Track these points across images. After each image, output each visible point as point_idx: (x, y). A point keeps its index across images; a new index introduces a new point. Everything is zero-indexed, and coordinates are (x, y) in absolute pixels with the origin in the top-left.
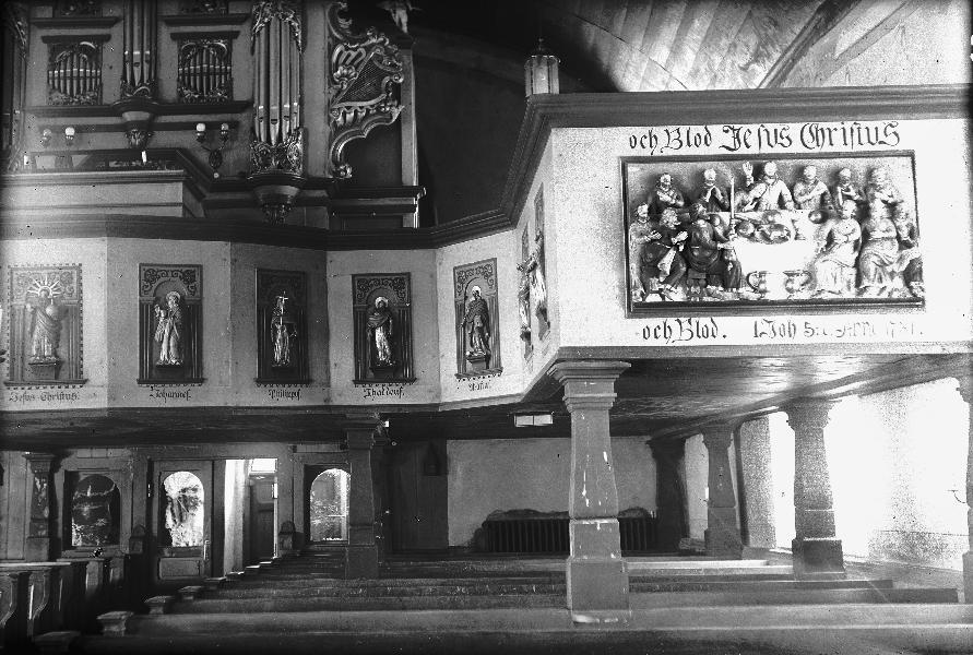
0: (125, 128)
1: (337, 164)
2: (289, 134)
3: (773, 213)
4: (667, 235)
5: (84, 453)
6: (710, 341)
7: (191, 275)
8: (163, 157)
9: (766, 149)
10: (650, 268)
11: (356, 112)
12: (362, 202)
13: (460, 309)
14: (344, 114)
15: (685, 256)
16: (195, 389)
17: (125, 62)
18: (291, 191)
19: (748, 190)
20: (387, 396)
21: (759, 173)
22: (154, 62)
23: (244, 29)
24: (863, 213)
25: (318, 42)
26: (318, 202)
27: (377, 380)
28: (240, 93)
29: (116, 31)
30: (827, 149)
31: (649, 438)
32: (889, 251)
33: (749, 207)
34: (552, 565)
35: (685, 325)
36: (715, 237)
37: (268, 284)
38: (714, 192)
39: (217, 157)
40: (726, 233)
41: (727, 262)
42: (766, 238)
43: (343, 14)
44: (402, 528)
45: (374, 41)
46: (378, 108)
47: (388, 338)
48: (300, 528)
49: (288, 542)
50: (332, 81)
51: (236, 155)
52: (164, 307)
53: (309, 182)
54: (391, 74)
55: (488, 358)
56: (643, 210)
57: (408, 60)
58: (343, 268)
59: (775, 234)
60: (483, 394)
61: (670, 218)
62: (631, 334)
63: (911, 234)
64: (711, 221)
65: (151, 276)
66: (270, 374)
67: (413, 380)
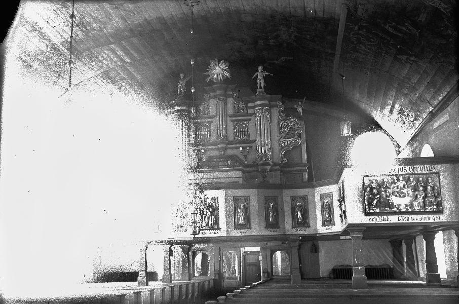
0: (218, 149)
1: (282, 158)
2: (268, 150)
3: (402, 189)
4: (374, 195)
5: (197, 245)
6: (387, 222)
7: (247, 199)
8: (233, 157)
10: (370, 204)
11: (287, 142)
12: (290, 169)
13: (322, 206)
14: (284, 143)
15: (379, 201)
16: (249, 231)
17: (218, 130)
18: (268, 167)
19: (395, 183)
20: (301, 231)
21: (398, 180)
22: (226, 129)
23: (252, 118)
24: (425, 190)
25: (275, 121)
26: (276, 170)
27: (299, 227)
28: (252, 138)
29: (214, 120)
30: (416, 172)
31: (389, 240)
32: (432, 199)
33: (396, 188)
34: (349, 282)
35: (380, 218)
36: (387, 196)
37: (267, 200)
38: (386, 184)
39: (246, 157)
40: (390, 195)
41: (390, 203)
42: (400, 196)
43: (282, 112)
44: (304, 271)
45: (292, 120)
46: (294, 141)
47: (301, 215)
48: (270, 271)
49: (266, 275)
50: (280, 133)
51: (251, 158)
52: (240, 208)
53: (275, 164)
54: (297, 130)
55: (331, 221)
56: (368, 189)
57: (303, 123)
58: (287, 195)
59: (402, 195)
60: (330, 231)
61: (375, 191)
62: (366, 220)
63: (438, 195)
64: (386, 192)
65: (236, 199)
66: (269, 226)
67: (309, 227)
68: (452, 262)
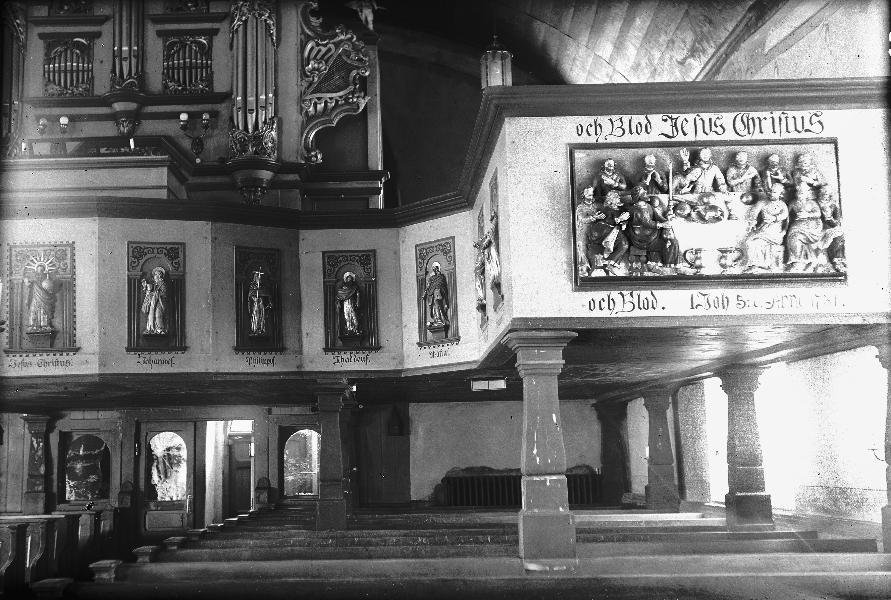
1: (309, 151)
2: (265, 122)
3: (708, 195)
4: (611, 215)
5: (77, 415)
6: (650, 313)
7: (175, 252)
8: (149, 144)
10: (595, 245)
11: (326, 102)
12: (332, 185)
13: (421, 283)
14: (315, 105)
15: (627, 235)
16: (179, 357)
17: (114, 57)
18: (266, 175)
19: (685, 174)
20: (354, 363)
21: (695, 159)
22: (141, 56)
23: (224, 26)
24: (791, 196)
25: (291, 38)
26: (291, 185)
27: (345, 348)
28: (220, 85)
30: (757, 136)
31: (594, 401)
32: (814, 230)
33: (686, 190)
34: (505, 517)
35: (628, 298)
36: (655, 217)
37: (246, 260)
38: (653, 176)
39: (198, 144)
40: (665, 214)
41: (666, 240)
42: (702, 218)
43: (314, 13)
44: (368, 483)
45: (342, 37)
46: (346, 99)
47: (356, 309)
48: (274, 484)
49: (264, 496)
50: (304, 74)
51: (216, 142)
52: (151, 281)
53: (283, 167)
54: (358, 68)
55: (446, 328)
56: (589, 192)
57: (374, 55)
58: (314, 246)
59: (710, 215)
60: (443, 361)
61: (614, 200)
62: (578, 306)
63: (834, 214)
64: (651, 203)
65: (138, 252)
66: (247, 342)
67: (378, 348)
68: (220, 461)
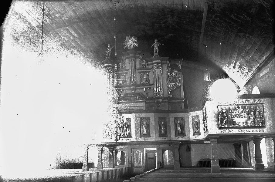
0: (131, 89)
1: (169, 95)
2: (160, 90)
3: (241, 113)
4: (224, 117)
5: (118, 147)
6: (232, 133)
7: (148, 119)
9: (240, 103)
10: (222, 122)
11: (172, 85)
12: (174, 101)
13: (193, 123)
14: (170, 86)
15: (227, 120)
16: (149, 138)
17: (130, 78)
18: (161, 100)
19: (237, 110)
20: (181, 139)
21: (238, 108)
22: (135, 77)
23: (151, 70)
24: (255, 113)
25: (165, 72)
26: (166, 102)
27: (179, 136)
28: (151, 82)
30: (249, 103)
31: (233, 144)
32: (259, 119)
33: (237, 112)
34: (209, 169)
35: (228, 130)
36: (232, 117)
37: (160, 120)
38: (231, 110)
39: (147, 94)
40: (234, 117)
41: (233, 121)
42: (240, 118)
43: (169, 67)
45: (175, 72)
46: (176, 84)
47: (181, 128)
48: (161, 162)
49: (159, 165)
50: (168, 79)
51: (150, 94)
52: (144, 125)
53: (165, 98)
54: (178, 78)
55: (198, 132)
56: (221, 113)
57: (181, 74)
58: (172, 117)
59: (241, 117)
60: (197, 138)
61: (225, 114)
62: (219, 132)
63: (262, 116)
64: (231, 115)
65: (141, 119)
66: (161, 135)
67: (185, 136)
